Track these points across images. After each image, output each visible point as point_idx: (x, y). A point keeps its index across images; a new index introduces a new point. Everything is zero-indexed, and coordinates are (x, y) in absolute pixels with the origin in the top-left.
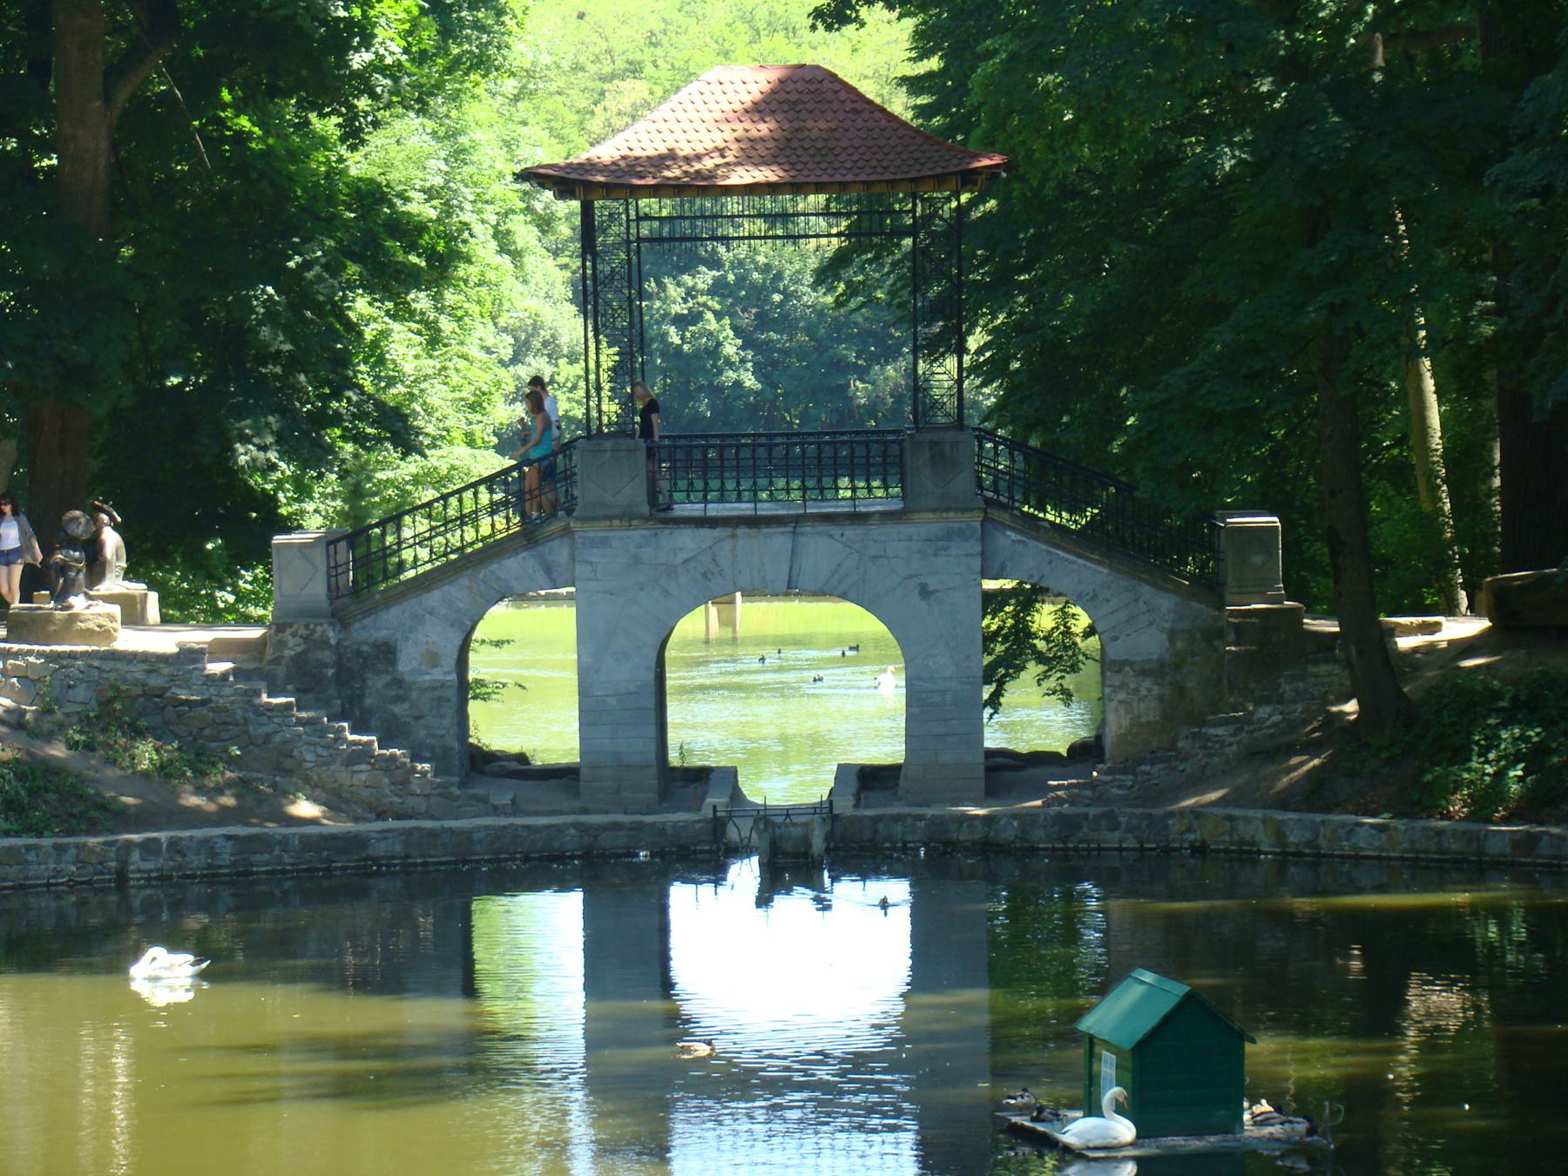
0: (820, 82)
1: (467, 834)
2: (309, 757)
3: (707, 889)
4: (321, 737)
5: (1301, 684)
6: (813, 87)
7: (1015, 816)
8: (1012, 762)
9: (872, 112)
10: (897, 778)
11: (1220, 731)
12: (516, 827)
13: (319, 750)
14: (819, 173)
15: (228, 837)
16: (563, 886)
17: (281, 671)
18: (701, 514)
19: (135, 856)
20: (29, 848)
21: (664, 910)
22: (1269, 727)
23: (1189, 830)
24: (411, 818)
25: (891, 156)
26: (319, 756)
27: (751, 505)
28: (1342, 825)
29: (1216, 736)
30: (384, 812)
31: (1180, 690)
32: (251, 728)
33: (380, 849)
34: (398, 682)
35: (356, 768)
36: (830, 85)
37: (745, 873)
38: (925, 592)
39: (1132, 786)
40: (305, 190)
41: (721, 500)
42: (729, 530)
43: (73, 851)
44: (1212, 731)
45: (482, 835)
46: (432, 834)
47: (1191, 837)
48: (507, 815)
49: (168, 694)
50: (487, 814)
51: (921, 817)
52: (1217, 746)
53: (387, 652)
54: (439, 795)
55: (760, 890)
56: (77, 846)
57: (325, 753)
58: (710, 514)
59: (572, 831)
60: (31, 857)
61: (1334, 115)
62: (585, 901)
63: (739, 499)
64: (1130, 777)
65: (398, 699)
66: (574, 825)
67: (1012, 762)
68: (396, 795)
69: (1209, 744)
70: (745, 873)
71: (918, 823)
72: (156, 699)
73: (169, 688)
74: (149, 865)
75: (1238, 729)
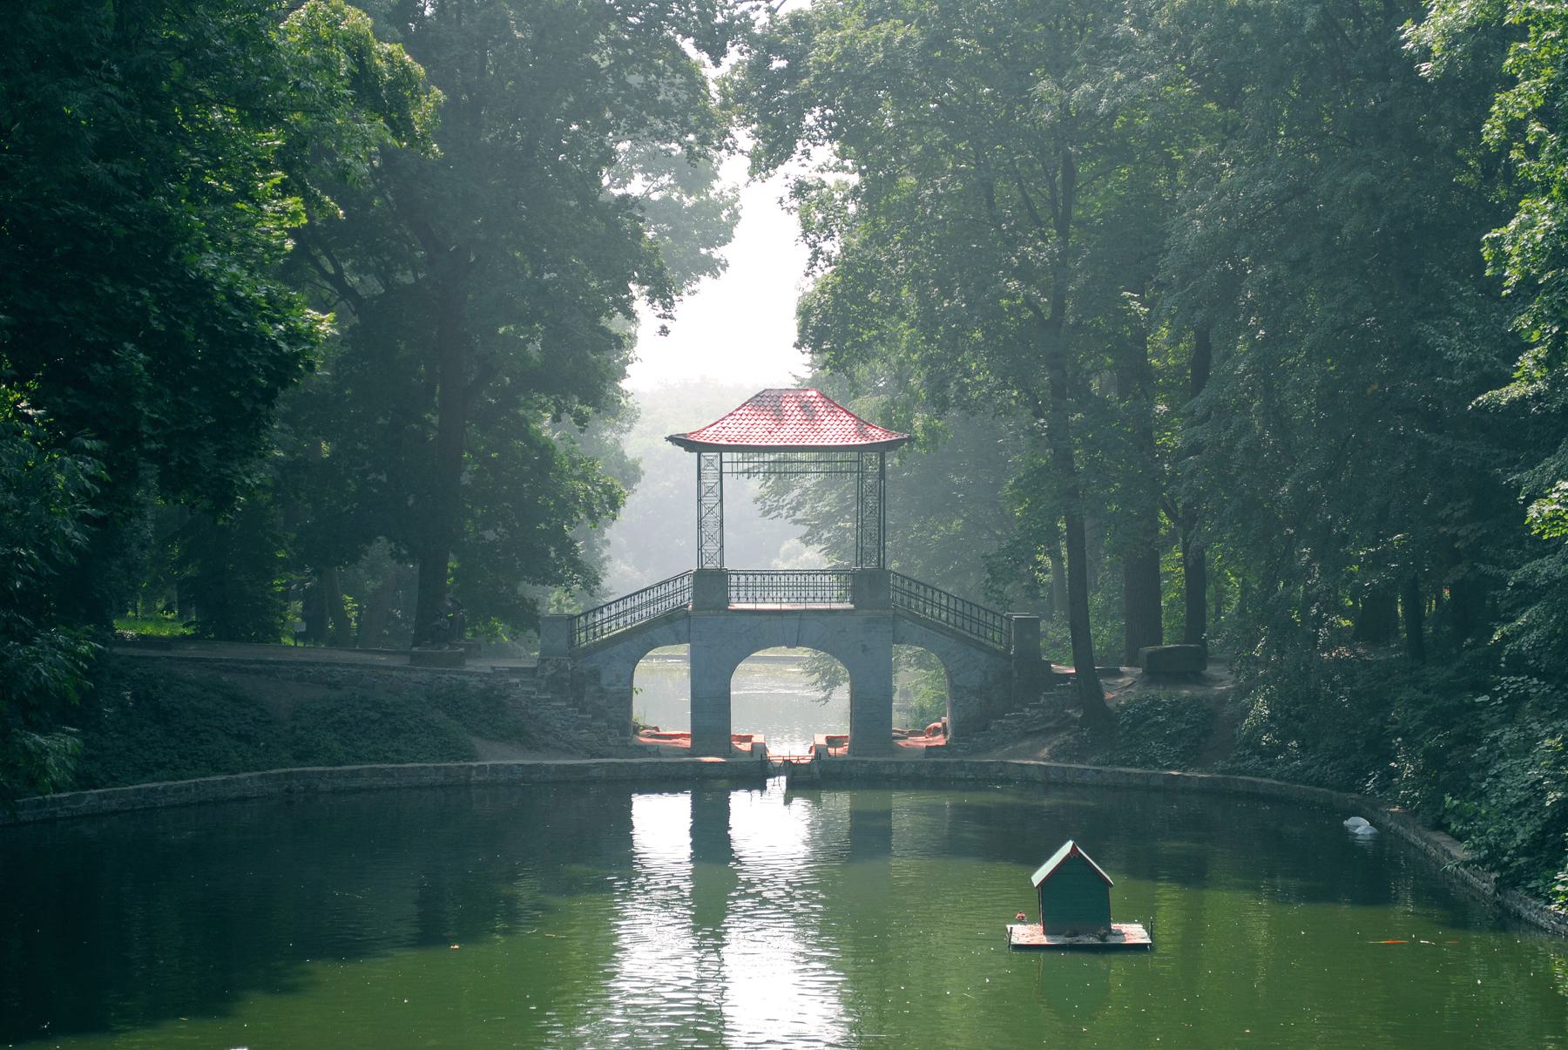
1: (640, 764)
2: (559, 725)
3: (756, 793)
15: (519, 765)
16: (630, 804)
17: (544, 683)
19: (474, 773)
20: (422, 768)
23: (1000, 771)
31: (875, 225)
33: (594, 773)
34: (601, 690)
37: (777, 785)
38: (865, 649)
41: (764, 602)
42: (768, 617)
43: (443, 770)
45: (645, 766)
46: (620, 765)
47: (1001, 774)
48: (654, 757)
51: (865, 762)
53: (596, 675)
55: (156, 1013)
56: (445, 767)
57: (566, 723)
60: (422, 773)
65: (601, 698)
70: (777, 785)
74: (481, 778)
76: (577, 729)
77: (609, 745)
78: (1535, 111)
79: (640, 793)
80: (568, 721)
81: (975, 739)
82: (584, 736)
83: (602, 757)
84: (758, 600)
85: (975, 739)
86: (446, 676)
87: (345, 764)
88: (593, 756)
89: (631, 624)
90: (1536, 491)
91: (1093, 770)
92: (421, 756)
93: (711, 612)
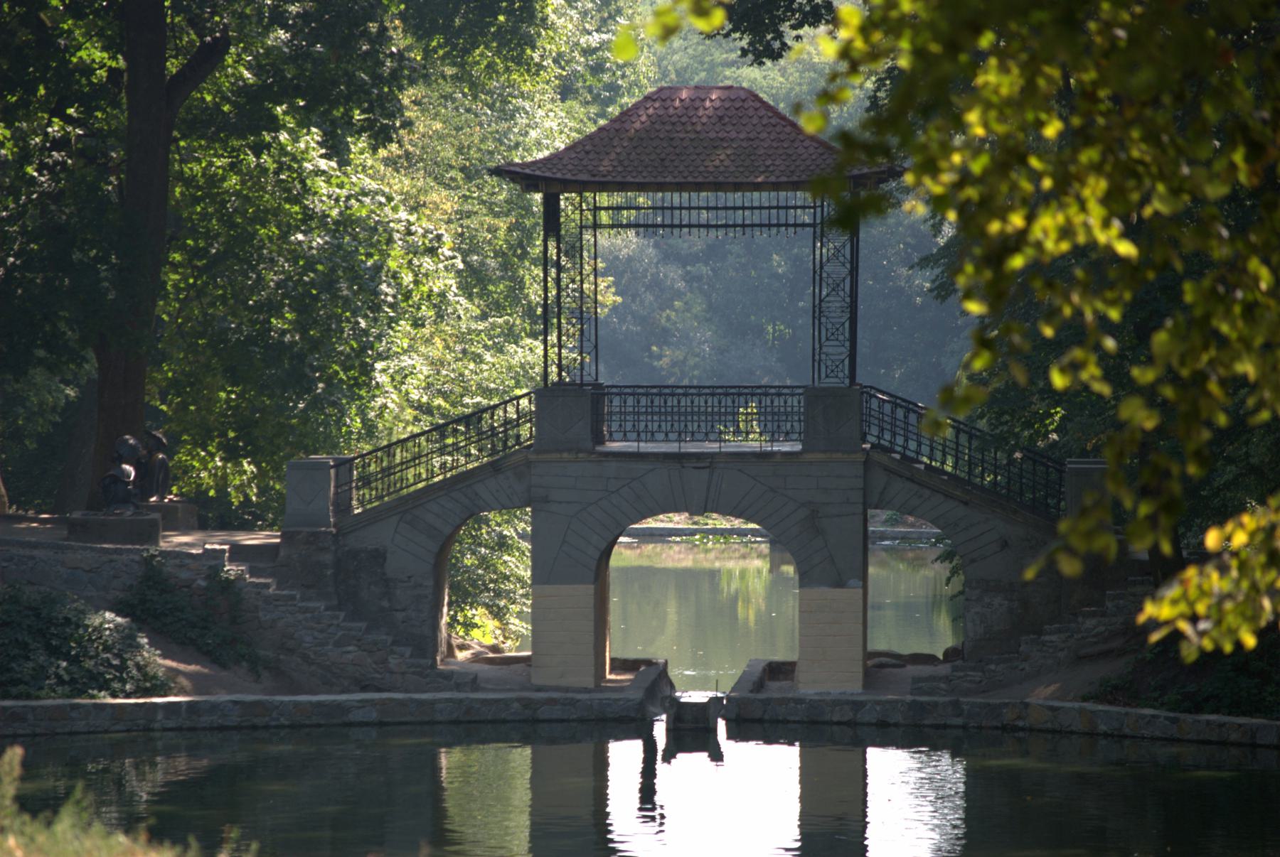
0: (743, 101)
1: (433, 703)
2: (308, 639)
4: (319, 623)
5: (1121, 602)
6: (738, 105)
7: (878, 703)
8: (894, 661)
9: (784, 126)
10: (793, 671)
11: (1054, 638)
12: (473, 700)
13: (316, 634)
14: (737, 174)
15: (235, 703)
18: (676, 450)
21: (864, 761)
22: (1094, 636)
24: (389, 691)
25: (798, 163)
26: (315, 638)
27: (676, 445)
28: (1143, 717)
29: (1052, 642)
30: (367, 686)
32: (261, 614)
35: (345, 649)
36: (751, 103)
39: (980, 682)
40: (1220, 237)
44: (1047, 638)
49: (194, 586)
50: (451, 690)
52: (1051, 650)
54: (414, 673)
58: (642, 450)
59: (516, 705)
60: (74, 714)
61: (249, 67)
62: (802, 756)
63: (667, 440)
64: (980, 674)
66: (518, 700)
67: (894, 661)
68: (378, 672)
69: (1045, 648)
71: (799, 706)
72: (185, 590)
73: (196, 580)
75: (1069, 637)
76: (338, 644)
77: (392, 672)
78: (386, 29)
79: (618, 739)
80: (322, 631)
81: (992, 667)
82: (350, 657)
83: (379, 690)
84: (643, 436)
85: (992, 667)
86: (124, 557)
87: (44, 699)
88: (364, 689)
89: (427, 479)
90: (215, 475)
91: (1167, 718)
92: (14, 691)
93: (565, 455)
